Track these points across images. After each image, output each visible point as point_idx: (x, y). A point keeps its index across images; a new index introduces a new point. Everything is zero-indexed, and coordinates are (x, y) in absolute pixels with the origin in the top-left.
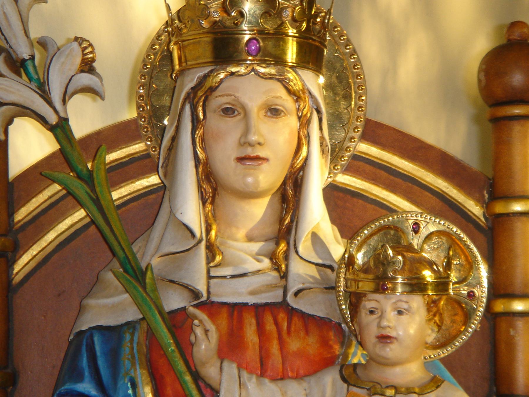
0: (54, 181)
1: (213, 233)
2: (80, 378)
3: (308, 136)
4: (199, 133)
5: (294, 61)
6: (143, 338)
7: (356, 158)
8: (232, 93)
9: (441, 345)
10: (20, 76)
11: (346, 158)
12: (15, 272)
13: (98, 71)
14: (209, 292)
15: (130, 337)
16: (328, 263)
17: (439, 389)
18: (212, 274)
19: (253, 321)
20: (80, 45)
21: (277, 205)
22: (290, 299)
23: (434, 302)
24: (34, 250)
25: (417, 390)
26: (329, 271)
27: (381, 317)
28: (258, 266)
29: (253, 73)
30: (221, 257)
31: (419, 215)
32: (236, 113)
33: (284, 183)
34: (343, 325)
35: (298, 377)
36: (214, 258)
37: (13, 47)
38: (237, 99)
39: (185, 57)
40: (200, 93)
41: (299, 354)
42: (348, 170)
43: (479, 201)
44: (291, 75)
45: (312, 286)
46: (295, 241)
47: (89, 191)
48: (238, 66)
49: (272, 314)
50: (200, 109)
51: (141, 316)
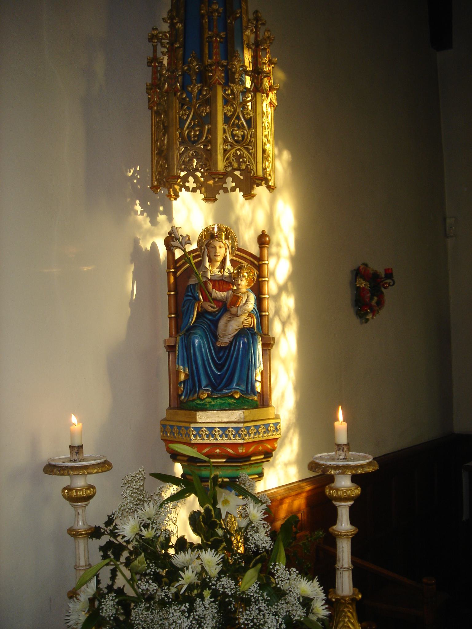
2: (189, 292)
3: (227, 251)
7: (236, 254)
28: (218, 273)
44: (223, 241)
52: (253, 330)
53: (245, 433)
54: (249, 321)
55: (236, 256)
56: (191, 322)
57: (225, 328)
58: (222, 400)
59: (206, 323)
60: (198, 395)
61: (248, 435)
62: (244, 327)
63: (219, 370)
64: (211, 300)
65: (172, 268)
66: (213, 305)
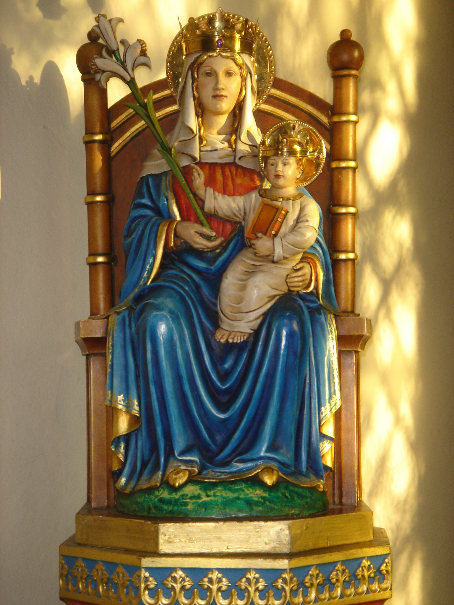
0: (130, 108)
1: (202, 131)
2: (143, 197)
3: (246, 85)
4: (195, 84)
5: (239, 50)
6: (171, 178)
7: (270, 96)
8: (210, 65)
9: (305, 180)
10: (112, 57)
11: (265, 96)
12: (112, 151)
13: (148, 55)
14: (200, 158)
15: (129, 417)
16: (254, 144)
17: (302, 198)
18: (202, 150)
19: (220, 170)
20: (140, 43)
21: (232, 118)
23: (300, 160)
24: (120, 141)
25: (292, 199)
26: (255, 148)
27: (276, 167)
29: (220, 56)
30: (206, 142)
31: (295, 121)
32: (212, 75)
33: (234, 108)
34: (261, 173)
35: (240, 195)
36: (202, 142)
37: (109, 44)
38: (212, 68)
39: (189, 48)
40: (195, 66)
41: (241, 185)
42: (266, 102)
43: (327, 116)
44: (237, 56)
45: (247, 155)
46: (239, 134)
48: (213, 52)
50: (196, 73)
51: (170, 169)
57: (241, 293)
58: (230, 490)
60: (163, 475)
63: (223, 407)
64: (202, 218)
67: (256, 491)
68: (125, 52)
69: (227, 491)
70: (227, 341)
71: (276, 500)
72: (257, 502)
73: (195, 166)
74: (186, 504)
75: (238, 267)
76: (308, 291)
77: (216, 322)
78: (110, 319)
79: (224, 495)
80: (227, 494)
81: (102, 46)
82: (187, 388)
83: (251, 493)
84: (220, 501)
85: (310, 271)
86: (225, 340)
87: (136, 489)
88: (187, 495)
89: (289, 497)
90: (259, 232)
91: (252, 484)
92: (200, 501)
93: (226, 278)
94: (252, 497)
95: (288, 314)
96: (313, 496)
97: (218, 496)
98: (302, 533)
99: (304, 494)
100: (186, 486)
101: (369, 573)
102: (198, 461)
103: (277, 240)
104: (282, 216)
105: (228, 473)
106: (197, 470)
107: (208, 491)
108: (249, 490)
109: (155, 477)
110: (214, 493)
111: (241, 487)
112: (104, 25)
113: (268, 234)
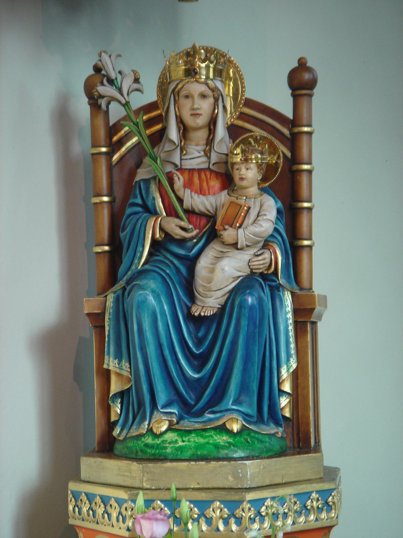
1: (183, 143)
4: (177, 105)
7: (241, 113)
14: (181, 165)
19: (197, 175)
22: (211, 167)
27: (240, 171)
38: (190, 91)
46: (213, 145)
47: (137, 128)
49: (204, 172)
52: (274, 278)
53: (252, 514)
54: (264, 259)
55: (242, 116)
56: (139, 263)
57: (211, 275)
58: (202, 436)
59: (172, 266)
60: (149, 425)
61: (257, 519)
62: (251, 272)
63: (198, 369)
64: (181, 213)
65: (103, 143)
66: (184, 224)
67: (222, 437)
68: (122, 81)
69: (199, 438)
70: (200, 314)
71: (239, 445)
72: (223, 446)
73: (176, 172)
74: (166, 448)
75: (210, 253)
76: (269, 272)
77: (192, 298)
78: (108, 297)
79: (197, 441)
80: (199, 440)
81: (104, 76)
82: (167, 353)
83: (218, 439)
84: (193, 445)
85: (270, 256)
86: (198, 313)
87: (127, 436)
88: (167, 441)
89: (251, 442)
90: (227, 224)
91: (219, 431)
92: (177, 446)
93: (200, 263)
94: (219, 442)
95: (248, 292)
96: (272, 441)
97: (192, 441)
98: (260, 472)
99: (263, 439)
100: (166, 434)
101: (317, 504)
102: (177, 413)
103: (241, 231)
104: (244, 211)
105: (201, 422)
106: (176, 421)
107: (183, 437)
108: (216, 436)
109: (142, 426)
110: (189, 439)
111: (211, 434)
112: (105, 59)
113: (233, 226)
